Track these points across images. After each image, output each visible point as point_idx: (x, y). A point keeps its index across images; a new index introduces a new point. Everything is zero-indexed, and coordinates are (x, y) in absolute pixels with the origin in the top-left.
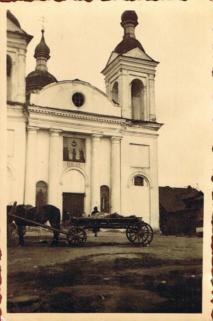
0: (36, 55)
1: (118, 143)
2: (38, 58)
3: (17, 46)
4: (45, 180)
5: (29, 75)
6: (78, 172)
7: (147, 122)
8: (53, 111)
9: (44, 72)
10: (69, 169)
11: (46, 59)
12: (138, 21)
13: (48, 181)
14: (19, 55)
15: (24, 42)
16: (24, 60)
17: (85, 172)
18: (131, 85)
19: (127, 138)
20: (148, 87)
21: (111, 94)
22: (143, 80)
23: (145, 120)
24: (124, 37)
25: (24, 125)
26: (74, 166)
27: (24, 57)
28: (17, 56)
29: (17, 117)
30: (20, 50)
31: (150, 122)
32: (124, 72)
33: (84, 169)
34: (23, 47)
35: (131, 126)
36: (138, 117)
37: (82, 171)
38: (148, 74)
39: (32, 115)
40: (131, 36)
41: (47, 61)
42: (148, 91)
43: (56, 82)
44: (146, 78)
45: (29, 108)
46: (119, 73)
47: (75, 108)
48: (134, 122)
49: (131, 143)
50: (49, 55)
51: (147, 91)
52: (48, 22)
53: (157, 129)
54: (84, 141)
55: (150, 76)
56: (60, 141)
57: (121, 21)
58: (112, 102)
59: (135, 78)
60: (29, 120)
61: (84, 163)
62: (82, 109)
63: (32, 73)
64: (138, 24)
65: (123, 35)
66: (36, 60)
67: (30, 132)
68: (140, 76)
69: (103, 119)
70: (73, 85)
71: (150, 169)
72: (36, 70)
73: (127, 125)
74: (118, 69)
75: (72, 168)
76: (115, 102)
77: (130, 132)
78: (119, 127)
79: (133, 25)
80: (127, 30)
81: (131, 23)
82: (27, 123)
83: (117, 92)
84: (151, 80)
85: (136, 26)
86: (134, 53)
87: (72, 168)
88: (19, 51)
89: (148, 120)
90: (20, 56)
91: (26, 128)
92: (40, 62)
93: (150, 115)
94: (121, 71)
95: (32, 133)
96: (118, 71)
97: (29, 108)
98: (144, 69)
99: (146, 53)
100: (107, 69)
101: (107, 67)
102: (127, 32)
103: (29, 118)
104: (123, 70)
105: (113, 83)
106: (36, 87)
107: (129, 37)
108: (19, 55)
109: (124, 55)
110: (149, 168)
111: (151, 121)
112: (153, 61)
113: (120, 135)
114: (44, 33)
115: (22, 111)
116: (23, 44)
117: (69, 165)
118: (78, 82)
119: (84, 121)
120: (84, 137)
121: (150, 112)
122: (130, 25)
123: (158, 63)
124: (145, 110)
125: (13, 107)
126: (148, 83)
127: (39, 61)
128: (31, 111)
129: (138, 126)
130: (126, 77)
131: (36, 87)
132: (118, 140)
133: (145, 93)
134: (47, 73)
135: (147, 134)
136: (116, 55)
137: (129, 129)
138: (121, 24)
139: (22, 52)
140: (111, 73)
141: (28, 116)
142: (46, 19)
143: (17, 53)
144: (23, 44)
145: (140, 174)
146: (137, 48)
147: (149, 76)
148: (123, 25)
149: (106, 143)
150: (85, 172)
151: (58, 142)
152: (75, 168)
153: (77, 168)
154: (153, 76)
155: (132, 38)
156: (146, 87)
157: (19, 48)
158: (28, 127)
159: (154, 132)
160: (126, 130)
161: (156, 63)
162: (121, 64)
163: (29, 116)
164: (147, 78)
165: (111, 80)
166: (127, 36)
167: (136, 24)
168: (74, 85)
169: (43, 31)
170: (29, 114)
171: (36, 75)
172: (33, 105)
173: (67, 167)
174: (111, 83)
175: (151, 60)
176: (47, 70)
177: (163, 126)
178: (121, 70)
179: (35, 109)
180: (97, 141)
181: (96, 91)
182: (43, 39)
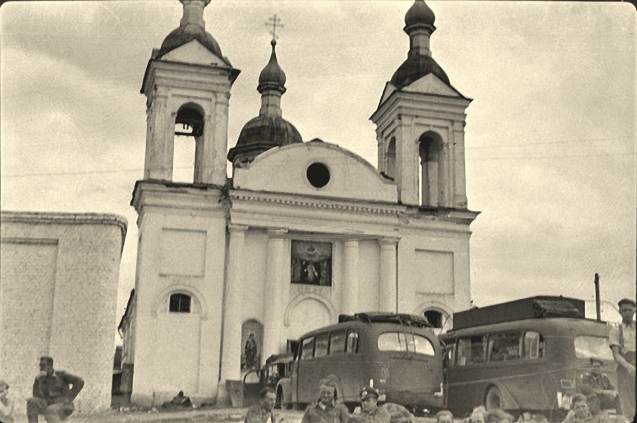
0: (262, 88)
1: (593, 301)
2: (264, 93)
3: (214, 88)
4: (258, 318)
5: (248, 123)
6: (317, 304)
7: (449, 210)
8: (266, 196)
9: (274, 118)
10: (301, 297)
11: (279, 94)
12: (435, 24)
13: (264, 315)
14: (216, 103)
15: (225, 80)
16: (226, 112)
17: (331, 303)
18: (420, 142)
19: (409, 241)
20: (451, 146)
21: (386, 160)
22: (442, 133)
23: (446, 206)
24: (410, 53)
25: (222, 223)
26: (310, 293)
27: (224, 106)
28: (213, 105)
29: (209, 209)
30: (218, 95)
31: (454, 209)
32: (405, 120)
33: (329, 298)
34: (224, 89)
35: (418, 218)
36: (434, 203)
37: (324, 300)
38: (452, 122)
39: (236, 206)
40: (422, 52)
41: (280, 97)
42: (451, 153)
43: (277, 147)
44: (447, 128)
45: (231, 193)
46: (397, 122)
47: (313, 191)
48: (426, 210)
49: (417, 248)
50: (285, 86)
51: (448, 153)
52: (282, 26)
53: (469, 222)
54: (330, 245)
55: (456, 124)
56: (287, 250)
57: (404, 25)
58: (381, 176)
59: (426, 129)
60: (232, 213)
61: (329, 287)
62: (324, 191)
63: (254, 121)
64: (435, 28)
65: (408, 49)
66: (261, 95)
67: (233, 234)
68: (435, 125)
69: (358, 206)
70: (309, 150)
71: (456, 295)
72: (260, 114)
73: (410, 216)
74: (395, 115)
75: (307, 296)
76: (386, 177)
77: (417, 228)
78: (395, 221)
79: (426, 32)
80: (414, 41)
81: (423, 28)
82: (228, 219)
83: (394, 155)
84: (457, 131)
85: (431, 32)
86: (427, 83)
87: (307, 296)
88: (216, 96)
89: (451, 206)
90: (218, 106)
91: (227, 228)
92: (268, 100)
93: (455, 195)
94: (400, 118)
95: (238, 238)
96: (395, 119)
97: (231, 193)
98: (444, 112)
99: (452, 83)
100: (379, 112)
101: (379, 108)
102: (414, 45)
103: (231, 210)
104: (403, 117)
105: (390, 138)
106: (258, 146)
107: (418, 54)
108: (216, 103)
109: (405, 89)
110: (454, 294)
111: (457, 206)
112: (461, 97)
113: (395, 234)
114: (276, 47)
115: (218, 199)
116: (223, 85)
117: (301, 290)
118: (317, 143)
119: (176, 192)
120: (329, 242)
121: (454, 190)
122: (421, 31)
123: (471, 100)
124: (446, 187)
125: (205, 193)
126: (451, 137)
127: (266, 97)
128: (235, 199)
129: (431, 217)
130: (409, 129)
131: (258, 146)
132: (392, 244)
133: (446, 156)
134: (279, 119)
135: (448, 231)
136: (392, 88)
137: (413, 222)
138: (404, 29)
139: (221, 98)
140: (384, 122)
141: (229, 207)
142: (279, 20)
143: (214, 100)
144: (223, 85)
145: (435, 305)
146: (431, 75)
147: (453, 124)
148: (407, 30)
149: (370, 250)
150: (331, 303)
151: (282, 252)
152: (312, 296)
153: (318, 297)
154: (460, 125)
155: (423, 56)
156: (448, 145)
157: (218, 92)
158: (230, 226)
159: (461, 227)
160: (409, 225)
161: (467, 102)
162: (400, 107)
163: (231, 207)
164: (450, 130)
165: (386, 134)
166: (414, 53)
167: (431, 29)
168: (311, 151)
169: (273, 44)
170: (231, 203)
171: (259, 124)
172: (238, 188)
173: (297, 293)
174: (386, 138)
175: (455, 95)
176: (281, 113)
177: (479, 216)
178: (399, 117)
179: (241, 195)
180: (353, 247)
181: (350, 159)
182: (274, 56)
